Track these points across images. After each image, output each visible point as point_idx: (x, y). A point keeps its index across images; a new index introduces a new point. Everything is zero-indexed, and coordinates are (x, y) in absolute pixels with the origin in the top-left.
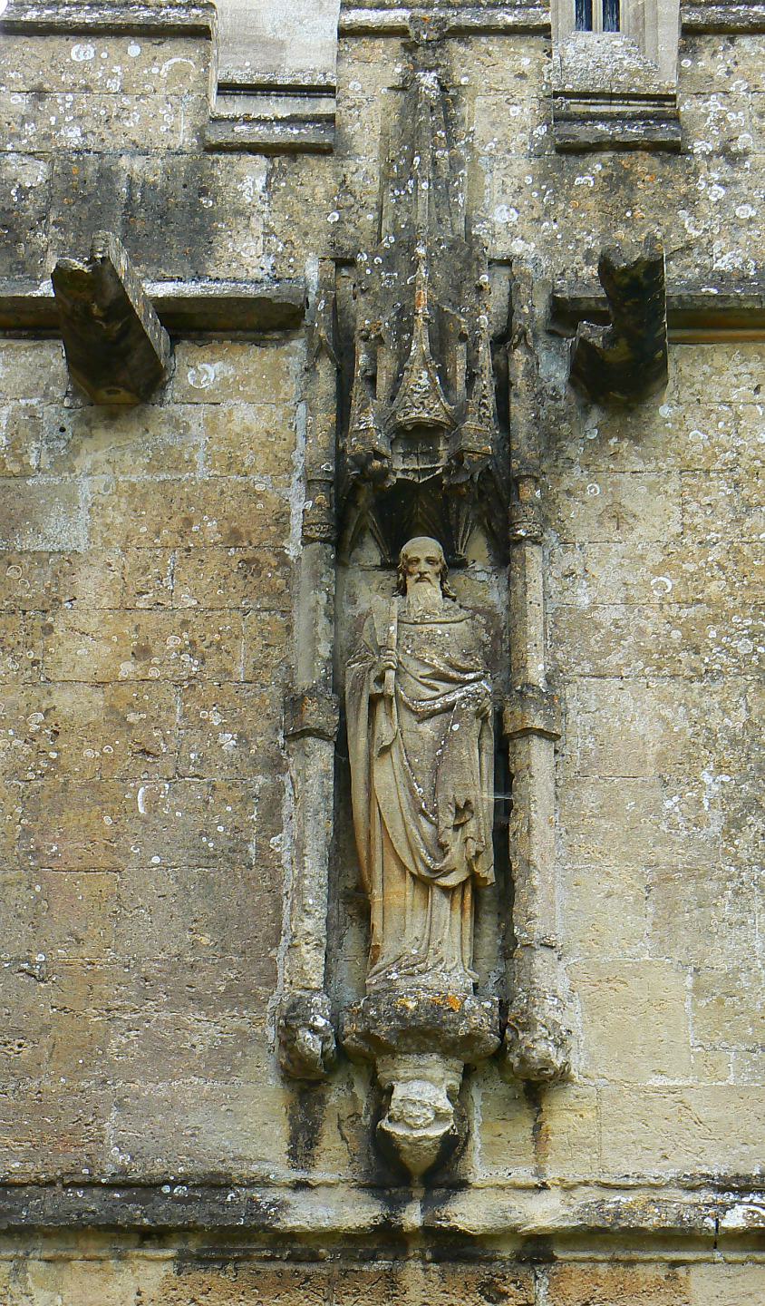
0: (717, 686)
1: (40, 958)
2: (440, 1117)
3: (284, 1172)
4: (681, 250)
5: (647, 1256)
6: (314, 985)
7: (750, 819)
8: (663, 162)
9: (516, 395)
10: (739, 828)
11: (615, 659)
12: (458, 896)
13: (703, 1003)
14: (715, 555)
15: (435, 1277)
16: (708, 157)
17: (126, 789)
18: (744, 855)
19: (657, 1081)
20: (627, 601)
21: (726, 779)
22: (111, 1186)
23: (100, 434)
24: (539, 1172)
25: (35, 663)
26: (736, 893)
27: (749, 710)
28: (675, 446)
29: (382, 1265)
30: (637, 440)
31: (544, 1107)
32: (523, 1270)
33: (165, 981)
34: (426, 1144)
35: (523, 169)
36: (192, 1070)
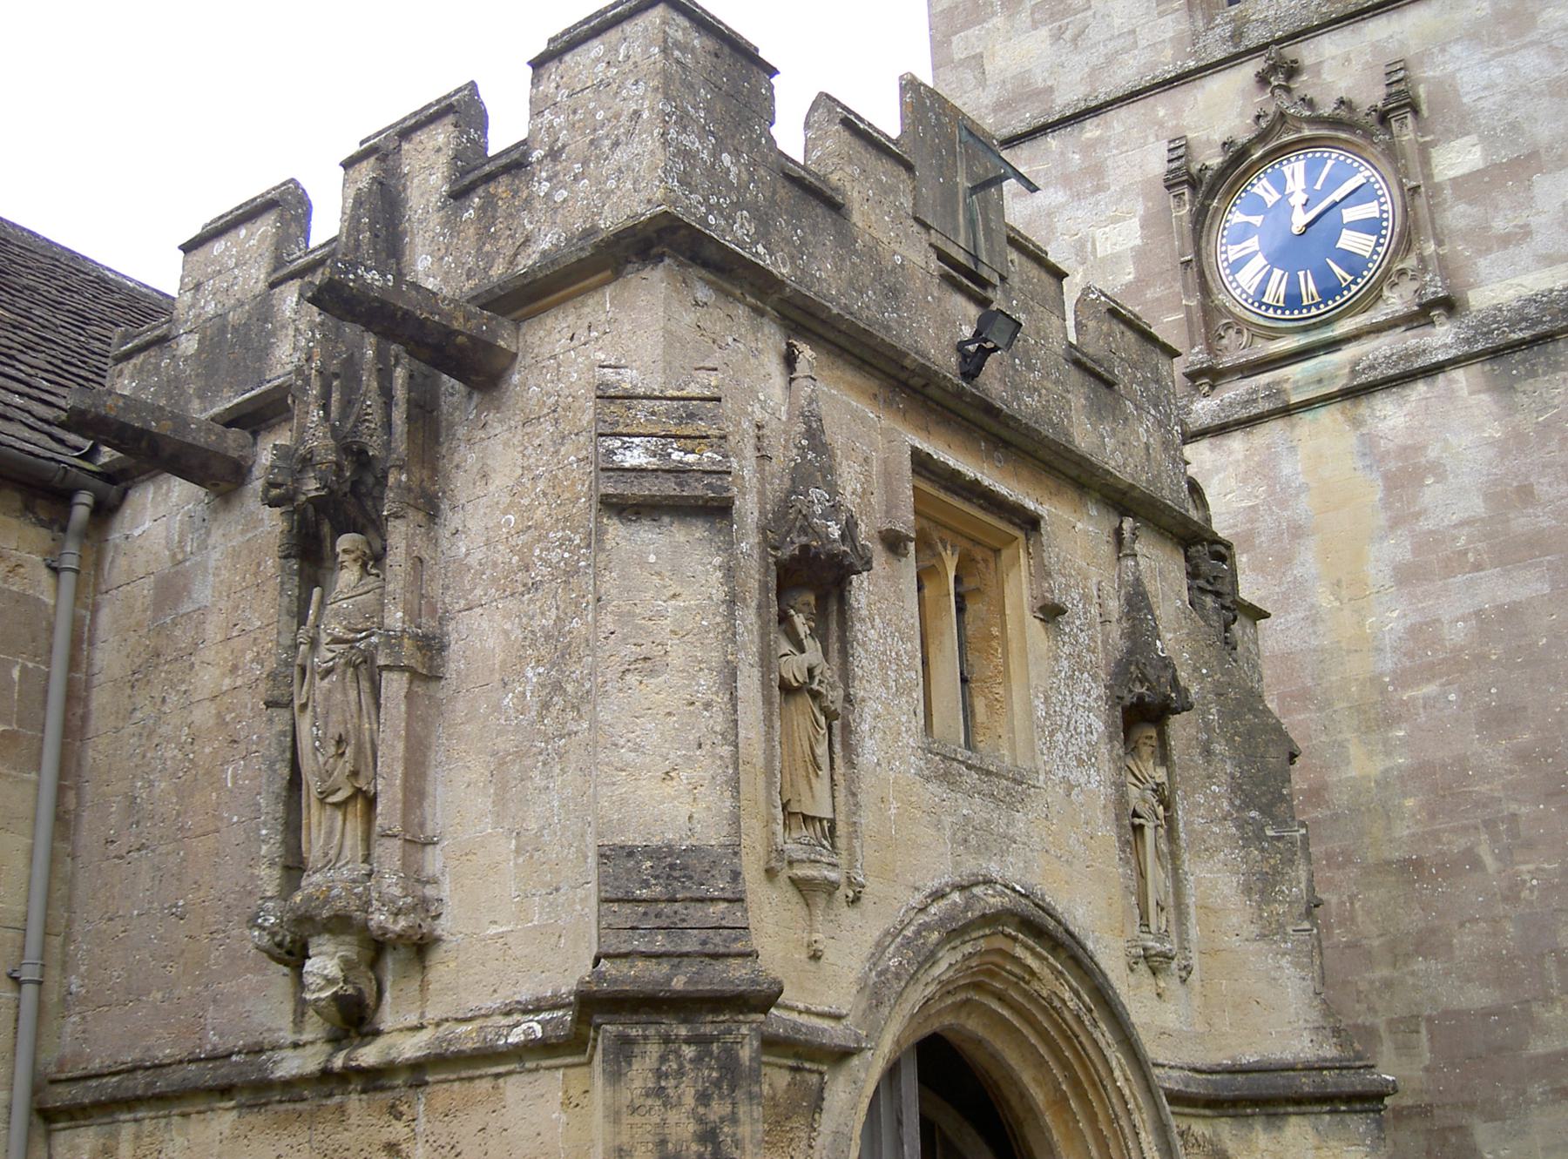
0: (539, 595)
1: (181, 903)
2: (330, 981)
3: (288, 1036)
4: (524, 243)
5: (478, 1073)
6: (269, 894)
7: (555, 699)
8: (516, 176)
9: (396, 405)
10: (547, 709)
11: (479, 592)
12: (350, 809)
13: (520, 860)
14: (541, 486)
15: (364, 1104)
16: (540, 162)
17: (223, 771)
18: (550, 731)
19: (493, 930)
20: (487, 543)
21: (541, 670)
22: (207, 1059)
23: (221, 516)
24: (422, 1015)
25: (185, 692)
26: (544, 764)
27: (557, 609)
28: (520, 405)
29: (337, 1099)
30: (498, 409)
31: (427, 964)
32: (411, 1092)
33: (237, 906)
34: (323, 1003)
35: (435, 219)
36: (247, 970)
